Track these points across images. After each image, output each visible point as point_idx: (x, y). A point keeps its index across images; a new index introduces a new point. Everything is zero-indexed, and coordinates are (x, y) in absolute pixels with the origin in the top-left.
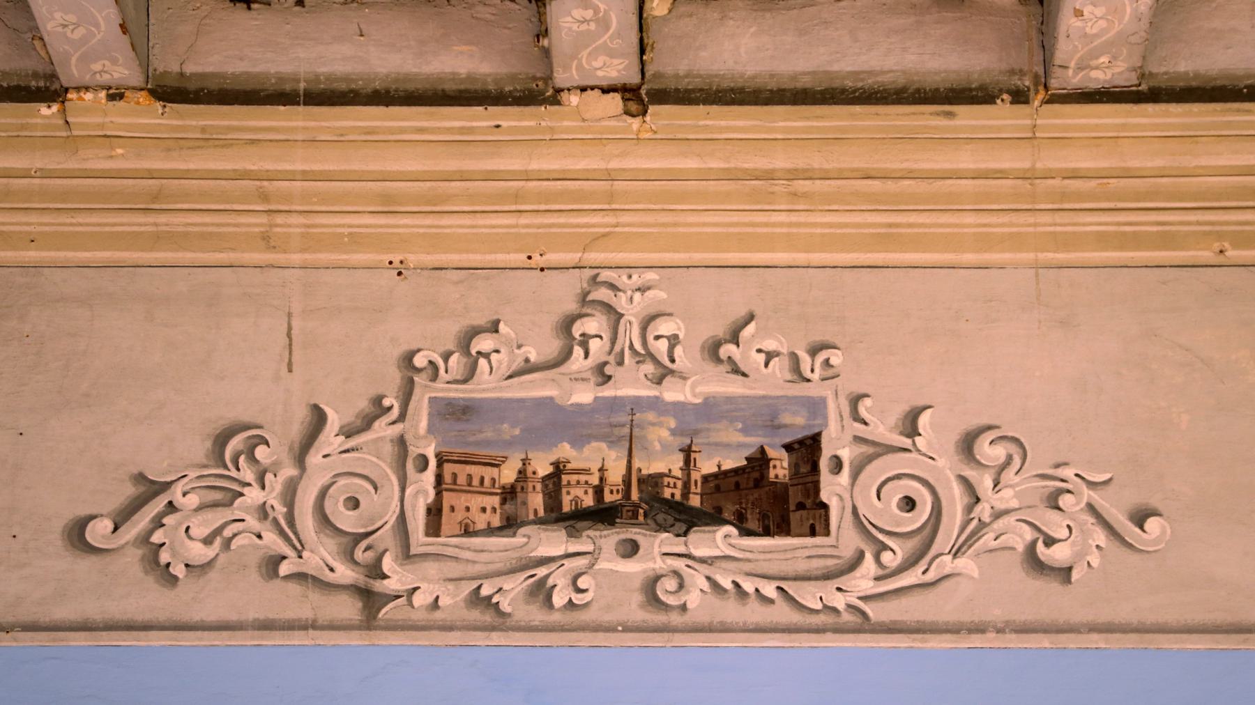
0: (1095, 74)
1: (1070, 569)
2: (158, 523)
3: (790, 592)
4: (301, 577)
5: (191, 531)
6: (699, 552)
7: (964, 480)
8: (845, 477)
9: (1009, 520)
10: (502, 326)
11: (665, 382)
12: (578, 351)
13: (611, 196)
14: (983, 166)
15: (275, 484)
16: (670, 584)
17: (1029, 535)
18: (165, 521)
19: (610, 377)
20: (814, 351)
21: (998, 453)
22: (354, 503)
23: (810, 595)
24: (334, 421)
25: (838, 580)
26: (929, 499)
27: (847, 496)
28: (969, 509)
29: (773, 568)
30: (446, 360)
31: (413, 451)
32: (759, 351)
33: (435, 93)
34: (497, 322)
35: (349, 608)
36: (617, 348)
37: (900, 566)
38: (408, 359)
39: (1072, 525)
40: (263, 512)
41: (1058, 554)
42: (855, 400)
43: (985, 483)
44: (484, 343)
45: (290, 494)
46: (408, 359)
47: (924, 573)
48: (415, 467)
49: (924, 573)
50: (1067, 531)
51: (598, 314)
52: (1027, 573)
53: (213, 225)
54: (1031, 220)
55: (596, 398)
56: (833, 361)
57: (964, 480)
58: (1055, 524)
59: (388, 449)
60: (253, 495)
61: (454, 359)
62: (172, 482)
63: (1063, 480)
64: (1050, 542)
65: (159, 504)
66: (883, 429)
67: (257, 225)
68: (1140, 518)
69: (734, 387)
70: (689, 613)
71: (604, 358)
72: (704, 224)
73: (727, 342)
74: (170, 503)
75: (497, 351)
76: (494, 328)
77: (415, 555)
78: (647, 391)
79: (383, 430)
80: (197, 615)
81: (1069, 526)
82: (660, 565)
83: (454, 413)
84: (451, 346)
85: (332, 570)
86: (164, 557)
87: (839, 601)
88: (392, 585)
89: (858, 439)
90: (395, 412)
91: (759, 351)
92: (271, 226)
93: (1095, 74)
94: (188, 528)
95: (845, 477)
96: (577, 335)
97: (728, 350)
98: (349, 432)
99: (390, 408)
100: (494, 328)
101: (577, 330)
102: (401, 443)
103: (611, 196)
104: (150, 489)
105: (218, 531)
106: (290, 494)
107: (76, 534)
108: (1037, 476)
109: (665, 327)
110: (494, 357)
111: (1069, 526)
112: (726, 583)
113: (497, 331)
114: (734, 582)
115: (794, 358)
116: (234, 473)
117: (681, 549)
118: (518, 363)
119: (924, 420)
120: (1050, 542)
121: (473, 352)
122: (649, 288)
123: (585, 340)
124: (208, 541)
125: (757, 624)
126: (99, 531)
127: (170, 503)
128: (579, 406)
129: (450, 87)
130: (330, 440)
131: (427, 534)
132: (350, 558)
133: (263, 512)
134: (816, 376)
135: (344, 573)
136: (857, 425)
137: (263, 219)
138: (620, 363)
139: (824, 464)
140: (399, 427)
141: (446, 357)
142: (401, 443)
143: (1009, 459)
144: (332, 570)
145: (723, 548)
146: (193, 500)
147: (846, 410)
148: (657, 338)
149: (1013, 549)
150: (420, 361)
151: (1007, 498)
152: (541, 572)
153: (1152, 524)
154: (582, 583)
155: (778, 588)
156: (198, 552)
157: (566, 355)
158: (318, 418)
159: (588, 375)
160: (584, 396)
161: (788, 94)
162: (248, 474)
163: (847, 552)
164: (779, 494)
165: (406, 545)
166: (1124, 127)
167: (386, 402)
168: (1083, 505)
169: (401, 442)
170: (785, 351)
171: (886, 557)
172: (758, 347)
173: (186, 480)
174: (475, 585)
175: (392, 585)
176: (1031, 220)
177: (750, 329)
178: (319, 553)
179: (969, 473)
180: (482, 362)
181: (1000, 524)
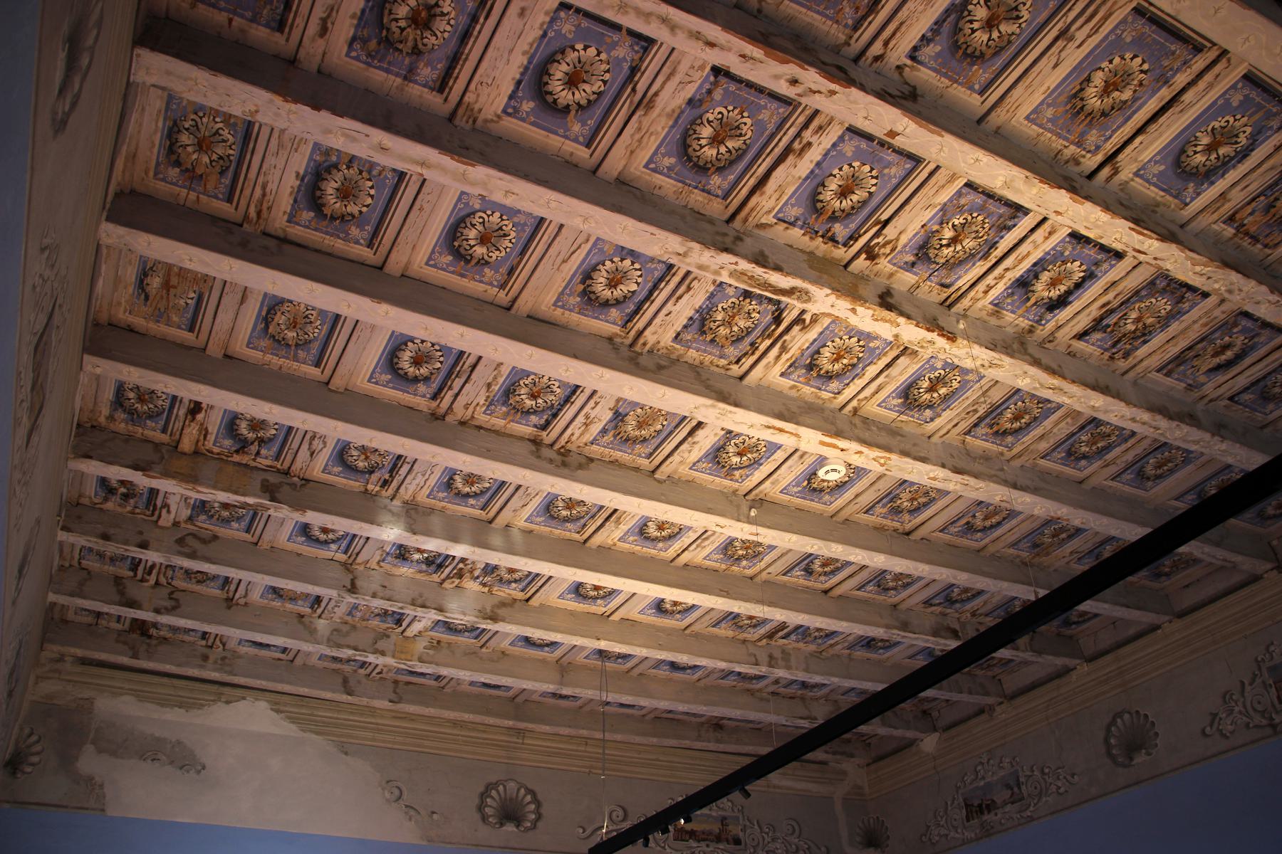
0: (1028, 500)
4: (1256, 726)
35: (1269, 731)
38: (1256, 660)
40: (1240, 712)
44: (1272, 648)
45: (1245, 707)
46: (1256, 660)
60: (1237, 709)
79: (1258, 681)
83: (1272, 669)
88: (1277, 721)
93: (1028, 500)
98: (1251, 684)
102: (1264, 682)
104: (1214, 715)
106: (1245, 707)
126: (1208, 729)
130: (1248, 688)
132: (1264, 717)
133: (1240, 712)
135: (1264, 722)
142: (1264, 682)
158: (1243, 683)
161: (176, 269)
164: (867, 252)
175: (1277, 721)
178: (1258, 719)
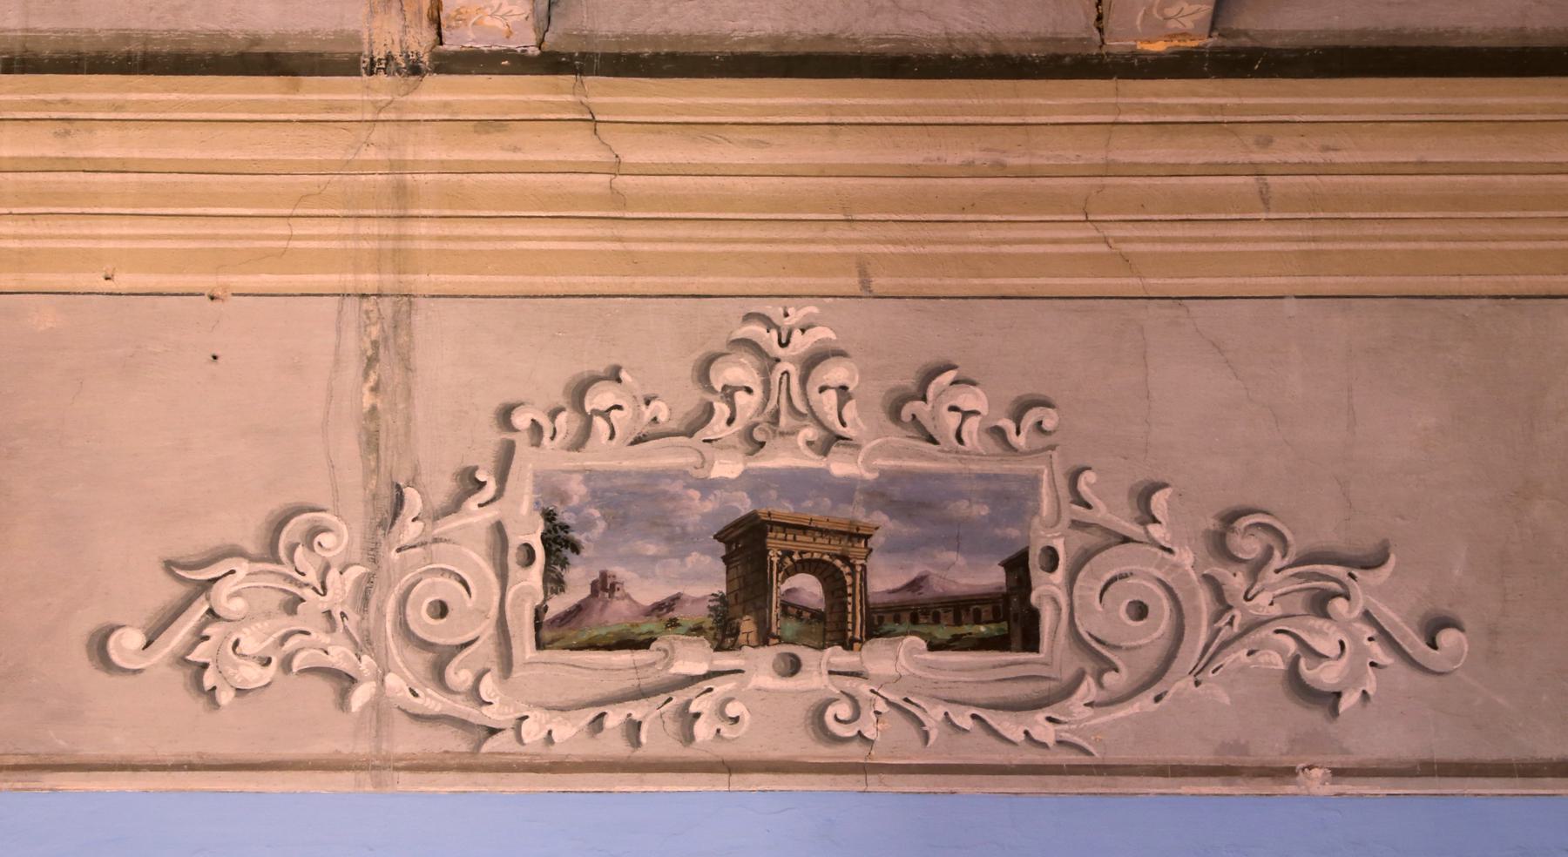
1: (1338, 695)
3: (990, 721)
7: (1209, 579)
8: (1059, 576)
9: (1266, 632)
10: (623, 375)
14: (32, 153)
16: (844, 710)
18: (207, 632)
19: (762, 444)
20: (1019, 410)
26: (1166, 604)
27: (1063, 600)
28: (1217, 617)
29: (966, 693)
31: (515, 540)
32: (953, 409)
34: (617, 369)
36: (771, 405)
41: (1326, 676)
42: (1074, 477)
43: (1236, 581)
45: (364, 595)
48: (518, 563)
55: (745, 473)
56: (1047, 425)
57: (1209, 579)
59: (484, 535)
61: (562, 418)
62: (215, 580)
65: (199, 610)
66: (1113, 513)
68: (1432, 629)
69: (924, 461)
70: (693, 745)
71: (756, 419)
73: (913, 398)
74: (211, 611)
75: (619, 407)
76: (614, 376)
78: (812, 461)
80: (89, 752)
81: (1342, 644)
82: (833, 687)
84: (562, 401)
86: (209, 679)
87: (1045, 732)
89: (1077, 524)
90: (491, 488)
91: (953, 409)
94: (236, 644)
95: (1059, 576)
96: (718, 387)
97: (914, 407)
99: (482, 485)
100: (614, 376)
107: (99, 646)
108: (1160, 580)
109: (835, 373)
111: (1342, 644)
118: (642, 428)
121: (588, 409)
122: (811, 326)
123: (729, 393)
127: (211, 611)
139: (1034, 560)
140: (491, 513)
141: (554, 414)
147: (1064, 491)
148: (822, 389)
150: (521, 420)
151: (1262, 604)
152: (679, 697)
153: (1447, 638)
154: (732, 710)
155: (974, 717)
156: (252, 675)
159: (736, 440)
163: (1068, 673)
166: (1394, 109)
168: (1357, 612)
169: (499, 529)
171: (1109, 678)
172: (953, 403)
174: (593, 713)
179: (1219, 571)
180: (599, 422)
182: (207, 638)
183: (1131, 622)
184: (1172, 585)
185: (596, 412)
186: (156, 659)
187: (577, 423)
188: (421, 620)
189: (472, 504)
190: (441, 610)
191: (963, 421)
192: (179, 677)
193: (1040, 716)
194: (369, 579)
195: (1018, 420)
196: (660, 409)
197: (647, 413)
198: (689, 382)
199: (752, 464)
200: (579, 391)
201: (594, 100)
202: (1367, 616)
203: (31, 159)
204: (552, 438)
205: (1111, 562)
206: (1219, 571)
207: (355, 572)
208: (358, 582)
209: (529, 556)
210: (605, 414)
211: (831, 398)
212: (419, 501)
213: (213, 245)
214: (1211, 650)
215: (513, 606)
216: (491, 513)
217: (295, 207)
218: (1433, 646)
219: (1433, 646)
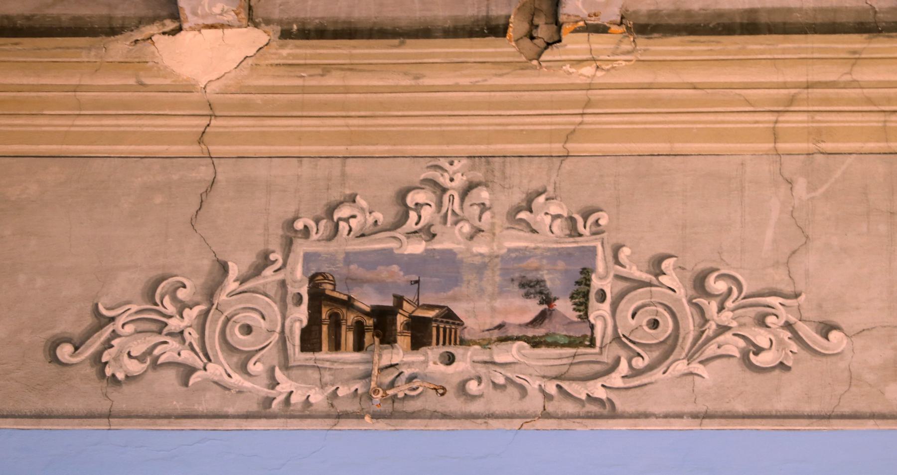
2: (108, 345)
5: (132, 354)
6: (498, 359)
8: (606, 306)
9: (728, 336)
10: (358, 198)
11: (475, 239)
12: (413, 215)
13: (588, 103)
14: (881, 78)
15: (191, 315)
17: (742, 343)
19: (434, 235)
21: (720, 287)
22: (248, 329)
23: (579, 390)
24: (234, 270)
25: (605, 378)
30: (317, 224)
31: (292, 290)
33: (680, 20)
37: (646, 367)
39: (773, 338)
43: (712, 307)
44: (344, 212)
47: (664, 373)
49: (664, 373)
50: (769, 343)
51: (427, 187)
52: (45, 346)
53: (483, 125)
54: (69, 123)
55: (426, 250)
58: (761, 338)
59: (272, 290)
61: (323, 223)
63: (769, 307)
64: (758, 350)
65: (107, 332)
67: (765, 122)
68: (826, 329)
72: (729, 122)
74: (114, 331)
77: (293, 367)
85: (229, 376)
89: (618, 277)
92: (776, 122)
95: (606, 306)
97: (523, 215)
101: (410, 200)
103: (80, 105)
105: (150, 351)
110: (352, 221)
112: (501, 380)
113: (354, 201)
114: (558, 386)
115: (572, 220)
116: (160, 308)
117: (486, 358)
119: (667, 265)
120: (758, 350)
124: (141, 359)
125: (724, 412)
126: (65, 352)
128: (412, 256)
129: (798, 18)
130: (231, 285)
131: (303, 349)
134: (586, 232)
136: (618, 267)
137: (772, 117)
138: (445, 222)
139: (592, 296)
140: (280, 276)
143: (730, 291)
144: (229, 376)
145: (516, 356)
146: (129, 329)
147: (610, 258)
149: (730, 356)
151: (726, 317)
156: (135, 367)
157: (406, 217)
158: (224, 268)
160: (417, 247)
162: (171, 309)
165: (286, 357)
167: (272, 257)
169: (283, 284)
170: (565, 215)
173: (129, 312)
176: (69, 123)
177: (541, 199)
179: (702, 301)
180: (342, 224)
181: (721, 339)
182: (112, 346)
183: (646, 329)
184: (670, 305)
185: (340, 219)
186: (82, 357)
187: (330, 225)
188: (237, 336)
189: (268, 272)
190: (248, 329)
191: (552, 221)
192: (90, 371)
193: (599, 383)
194: (207, 312)
195: (585, 220)
196: (379, 216)
197: (371, 220)
198: (324, 202)
199: (430, 247)
200: (331, 210)
201: (594, 46)
202: (788, 326)
203: (564, 85)
204: (317, 233)
205: (638, 298)
206: (702, 301)
207: (197, 310)
208: (198, 316)
209: (299, 299)
210: (347, 220)
211: (476, 210)
212: (236, 268)
213: (438, 129)
214: (700, 342)
215: (646, 311)
216: (280, 276)
217: (584, 108)
218: (827, 339)
219: (827, 339)
